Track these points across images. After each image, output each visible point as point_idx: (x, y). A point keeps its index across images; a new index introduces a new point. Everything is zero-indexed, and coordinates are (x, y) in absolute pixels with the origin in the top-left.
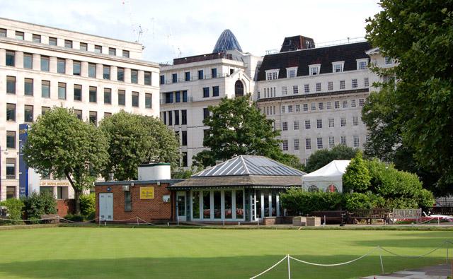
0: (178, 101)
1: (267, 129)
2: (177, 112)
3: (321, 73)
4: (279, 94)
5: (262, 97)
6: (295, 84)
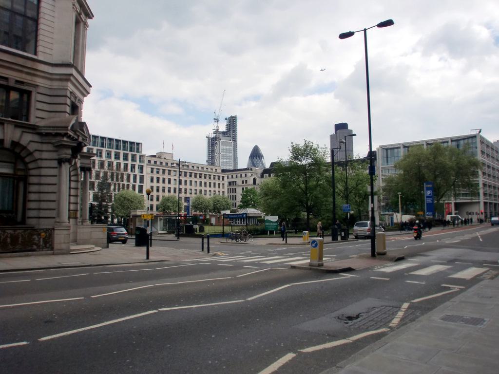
0: (233, 185)
2: (233, 189)
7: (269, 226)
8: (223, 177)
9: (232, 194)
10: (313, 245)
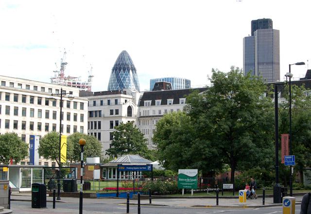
0: (96, 116)
1: (141, 138)
2: (95, 122)
3: (173, 104)
4: (151, 114)
5: (142, 115)
6: (160, 109)
7: (184, 182)
8: (82, 104)
9: (94, 131)
10: (286, 204)
